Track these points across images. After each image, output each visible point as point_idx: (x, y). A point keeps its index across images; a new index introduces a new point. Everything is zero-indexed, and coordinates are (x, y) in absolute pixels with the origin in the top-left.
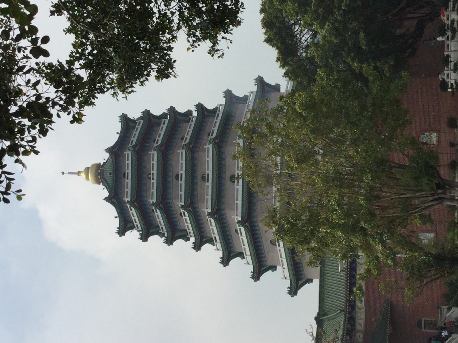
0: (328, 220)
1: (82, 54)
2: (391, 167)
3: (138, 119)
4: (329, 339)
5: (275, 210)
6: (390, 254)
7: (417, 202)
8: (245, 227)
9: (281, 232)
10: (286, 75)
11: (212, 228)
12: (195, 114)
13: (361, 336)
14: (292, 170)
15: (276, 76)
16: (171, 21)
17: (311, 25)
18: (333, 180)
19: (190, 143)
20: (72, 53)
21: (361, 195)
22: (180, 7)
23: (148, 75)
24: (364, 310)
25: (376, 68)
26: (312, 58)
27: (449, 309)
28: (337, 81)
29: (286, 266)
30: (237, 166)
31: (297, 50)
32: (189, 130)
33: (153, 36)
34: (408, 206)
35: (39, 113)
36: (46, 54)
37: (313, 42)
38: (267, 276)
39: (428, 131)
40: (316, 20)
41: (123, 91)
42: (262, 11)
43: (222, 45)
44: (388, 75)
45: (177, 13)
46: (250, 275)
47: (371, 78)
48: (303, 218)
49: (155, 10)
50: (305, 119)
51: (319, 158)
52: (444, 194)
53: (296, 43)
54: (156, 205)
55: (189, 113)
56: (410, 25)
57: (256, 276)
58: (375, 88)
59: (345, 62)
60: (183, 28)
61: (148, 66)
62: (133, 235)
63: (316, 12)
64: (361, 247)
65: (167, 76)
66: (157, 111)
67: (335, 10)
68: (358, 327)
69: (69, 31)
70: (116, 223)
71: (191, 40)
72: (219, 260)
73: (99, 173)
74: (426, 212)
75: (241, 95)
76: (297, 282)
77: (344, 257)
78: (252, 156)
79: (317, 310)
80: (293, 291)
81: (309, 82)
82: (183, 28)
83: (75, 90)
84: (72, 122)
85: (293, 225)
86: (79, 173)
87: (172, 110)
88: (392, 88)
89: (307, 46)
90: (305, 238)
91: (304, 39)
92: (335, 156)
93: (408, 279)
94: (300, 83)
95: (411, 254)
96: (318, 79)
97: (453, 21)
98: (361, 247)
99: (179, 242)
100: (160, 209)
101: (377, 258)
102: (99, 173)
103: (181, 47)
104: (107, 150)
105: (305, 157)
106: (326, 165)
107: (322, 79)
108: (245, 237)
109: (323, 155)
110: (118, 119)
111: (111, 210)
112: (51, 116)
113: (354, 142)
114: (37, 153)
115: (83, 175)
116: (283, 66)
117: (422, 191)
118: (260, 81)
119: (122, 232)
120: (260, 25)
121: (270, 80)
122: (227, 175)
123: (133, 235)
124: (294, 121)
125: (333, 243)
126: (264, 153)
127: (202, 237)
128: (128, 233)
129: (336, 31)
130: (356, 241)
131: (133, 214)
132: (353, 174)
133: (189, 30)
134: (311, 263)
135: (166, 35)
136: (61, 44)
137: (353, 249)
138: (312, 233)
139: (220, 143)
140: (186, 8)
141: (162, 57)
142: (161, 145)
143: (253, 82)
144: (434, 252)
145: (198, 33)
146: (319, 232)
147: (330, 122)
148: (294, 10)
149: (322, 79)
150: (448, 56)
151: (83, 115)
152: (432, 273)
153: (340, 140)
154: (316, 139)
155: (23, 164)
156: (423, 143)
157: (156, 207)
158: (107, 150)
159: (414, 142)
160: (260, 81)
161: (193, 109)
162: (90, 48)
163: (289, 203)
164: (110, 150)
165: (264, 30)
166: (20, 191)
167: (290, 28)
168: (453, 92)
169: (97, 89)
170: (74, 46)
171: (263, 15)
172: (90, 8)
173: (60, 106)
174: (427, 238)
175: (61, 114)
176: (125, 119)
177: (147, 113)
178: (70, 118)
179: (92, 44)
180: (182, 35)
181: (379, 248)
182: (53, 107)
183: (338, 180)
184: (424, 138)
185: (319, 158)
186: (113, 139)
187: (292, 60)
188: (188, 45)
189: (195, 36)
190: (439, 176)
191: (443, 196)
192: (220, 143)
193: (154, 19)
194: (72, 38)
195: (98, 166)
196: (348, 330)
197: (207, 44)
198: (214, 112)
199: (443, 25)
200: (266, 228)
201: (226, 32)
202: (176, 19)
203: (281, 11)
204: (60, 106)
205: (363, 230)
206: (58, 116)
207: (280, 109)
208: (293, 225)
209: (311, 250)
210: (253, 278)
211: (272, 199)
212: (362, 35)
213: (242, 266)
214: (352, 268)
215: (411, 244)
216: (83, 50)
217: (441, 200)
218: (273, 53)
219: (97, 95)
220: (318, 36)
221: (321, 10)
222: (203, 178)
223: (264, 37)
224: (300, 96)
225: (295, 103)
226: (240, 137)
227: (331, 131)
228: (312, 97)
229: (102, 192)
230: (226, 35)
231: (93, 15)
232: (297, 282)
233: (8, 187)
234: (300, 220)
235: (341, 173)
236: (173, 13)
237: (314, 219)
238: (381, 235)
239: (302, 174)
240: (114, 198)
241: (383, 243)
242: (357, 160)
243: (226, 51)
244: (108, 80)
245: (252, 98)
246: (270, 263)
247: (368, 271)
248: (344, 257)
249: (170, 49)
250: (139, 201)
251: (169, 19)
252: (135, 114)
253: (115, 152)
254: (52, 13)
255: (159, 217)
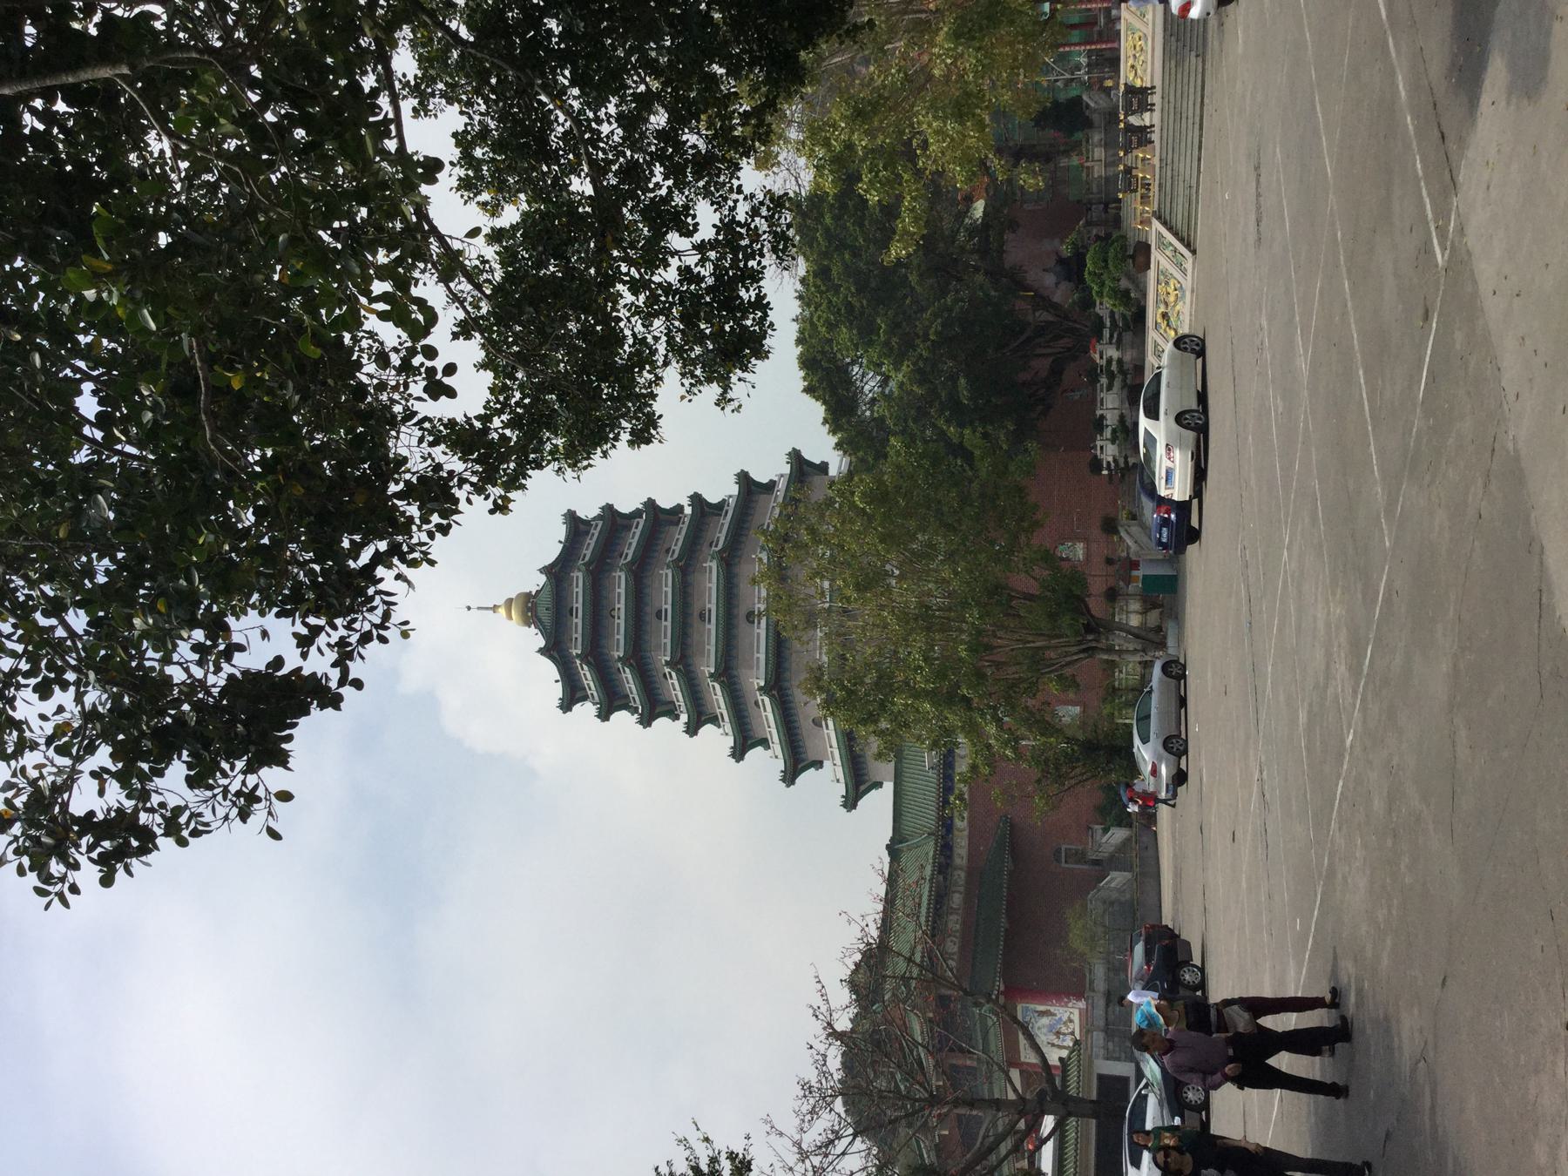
0: (907, 684)
1: (505, 405)
2: (1012, 598)
3: (594, 519)
4: (910, 881)
5: (820, 668)
6: (1009, 741)
7: (1053, 655)
8: (771, 697)
9: (830, 704)
10: (838, 446)
11: (717, 698)
12: (688, 510)
13: (963, 875)
14: (849, 602)
15: (823, 448)
16: (654, 352)
17: (880, 365)
18: (916, 619)
19: (679, 559)
20: (488, 402)
21: (963, 642)
22: (668, 328)
23: (616, 439)
24: (966, 833)
25: (985, 436)
26: (882, 419)
27: (1106, 831)
28: (922, 456)
29: (838, 761)
30: (757, 597)
31: (857, 407)
32: (677, 538)
33: (624, 377)
34: (1037, 662)
35: (436, 495)
36: (451, 393)
37: (883, 393)
38: (807, 777)
39: (1070, 539)
40: (887, 356)
41: (573, 466)
42: (799, 341)
43: (738, 390)
44: (1005, 447)
45: (664, 338)
46: (779, 775)
47: (977, 453)
48: (867, 680)
49: (627, 332)
50: (870, 518)
51: (893, 582)
52: (1097, 641)
53: (855, 394)
54: (624, 660)
55: (680, 508)
56: (1042, 366)
57: (790, 777)
58: (984, 468)
59: (934, 426)
60: (674, 363)
61: (615, 425)
62: (586, 711)
63: (887, 344)
64: (963, 728)
65: (648, 441)
66: (625, 507)
67: (918, 341)
68: (958, 861)
69: (483, 366)
70: (557, 691)
71: (687, 382)
72: (729, 752)
73: (528, 608)
74: (1068, 671)
75: (765, 480)
76: (857, 787)
77: (935, 745)
78: (783, 579)
79: (890, 834)
80: (850, 802)
81: (876, 459)
82: (674, 363)
83: (498, 460)
84: (492, 512)
85: (850, 693)
86: (495, 608)
87: (650, 504)
88: (1012, 468)
89: (873, 400)
90: (871, 714)
91: (867, 388)
92: (920, 579)
93: (1039, 781)
94: (862, 460)
95: (1043, 739)
96: (892, 453)
97: (1110, 361)
98: (963, 728)
99: (662, 723)
100: (630, 666)
101: (989, 747)
102: (528, 608)
103: (670, 392)
104: (541, 571)
105: (870, 581)
106: (904, 593)
107: (898, 453)
108: (772, 711)
109: (901, 578)
110: (733, 479)
111: (549, 670)
112: (456, 501)
113: (951, 557)
114: (432, 563)
115: (502, 611)
116: (833, 432)
117: (1061, 636)
118: (796, 457)
119: (567, 705)
120: (795, 364)
121: (813, 455)
122: (742, 611)
123: (586, 711)
124: (852, 522)
125: (917, 721)
126: (803, 574)
127: (700, 714)
128: (577, 708)
129: (921, 376)
130: (953, 719)
131: (587, 676)
132: (950, 609)
133: (684, 366)
134: (879, 756)
135: (645, 373)
136: (472, 393)
137: (948, 732)
138: (882, 705)
139: (730, 559)
140: (679, 330)
141: (640, 409)
142: (632, 562)
143: (785, 458)
144: (1081, 737)
145: (698, 372)
146: (893, 704)
147: (912, 524)
148: (851, 340)
149: (898, 453)
150: (1102, 417)
151: (510, 501)
152: (1078, 771)
153: (929, 552)
154: (888, 552)
155: (409, 583)
156: (1062, 559)
157: (624, 664)
158: (541, 571)
159: (1049, 558)
160: (796, 457)
161: (685, 502)
162: (518, 395)
163: (843, 657)
164: (546, 570)
165: (802, 374)
166: (406, 623)
167: (844, 370)
168: (1110, 475)
169: (529, 463)
170: (492, 390)
171: (800, 349)
172: (518, 328)
173: (472, 484)
174: (1069, 713)
175: (474, 498)
176: (572, 518)
177: (609, 510)
178: (489, 504)
179: (522, 387)
180: (672, 374)
181: (992, 729)
182: (460, 487)
183: (925, 619)
184: (1063, 551)
185: (893, 582)
186: (552, 552)
187: (849, 422)
188: (683, 391)
189: (693, 376)
190: (1089, 611)
191: (1094, 644)
192: (730, 559)
193: (626, 347)
194: (488, 377)
195: (527, 597)
196: (940, 865)
197: (714, 390)
198: (721, 506)
199: (1094, 365)
200: (805, 698)
201: (745, 369)
202: (662, 348)
203: (830, 341)
204: (472, 484)
205: (967, 701)
206: (469, 501)
207: (830, 502)
208: (850, 693)
209: (880, 734)
210: (783, 780)
211: (816, 650)
212: (962, 381)
213: (766, 761)
214: (947, 763)
215: (1047, 727)
216: (507, 398)
217: (1090, 651)
218: (817, 410)
219: (530, 472)
220: (892, 384)
221: (894, 340)
222: (702, 616)
223: (802, 384)
224: (861, 480)
225: (853, 493)
226: (763, 548)
227: (913, 538)
228: (880, 482)
229: (534, 639)
230: (745, 375)
231: (522, 339)
232: (857, 787)
233: (386, 616)
234: (862, 683)
235: (928, 608)
236: (656, 339)
237: (885, 683)
238: (995, 708)
239: (866, 611)
240: (554, 649)
241: (999, 721)
242: (955, 585)
243: (744, 401)
244: (548, 447)
245: (782, 485)
246: (812, 756)
247: (974, 768)
248: (935, 745)
249: (653, 396)
250: (596, 655)
251: (650, 348)
252: (588, 510)
253: (557, 572)
254: (455, 336)
255: (628, 680)
